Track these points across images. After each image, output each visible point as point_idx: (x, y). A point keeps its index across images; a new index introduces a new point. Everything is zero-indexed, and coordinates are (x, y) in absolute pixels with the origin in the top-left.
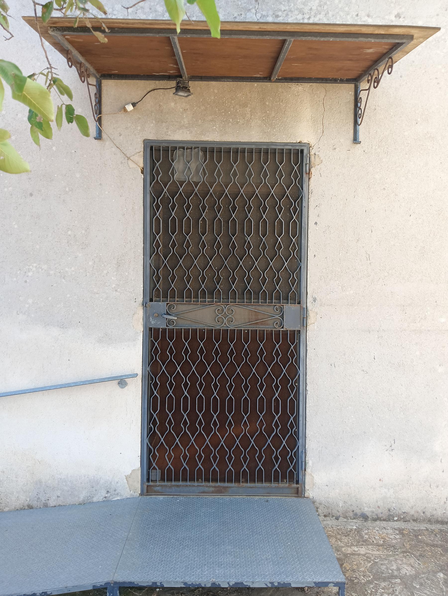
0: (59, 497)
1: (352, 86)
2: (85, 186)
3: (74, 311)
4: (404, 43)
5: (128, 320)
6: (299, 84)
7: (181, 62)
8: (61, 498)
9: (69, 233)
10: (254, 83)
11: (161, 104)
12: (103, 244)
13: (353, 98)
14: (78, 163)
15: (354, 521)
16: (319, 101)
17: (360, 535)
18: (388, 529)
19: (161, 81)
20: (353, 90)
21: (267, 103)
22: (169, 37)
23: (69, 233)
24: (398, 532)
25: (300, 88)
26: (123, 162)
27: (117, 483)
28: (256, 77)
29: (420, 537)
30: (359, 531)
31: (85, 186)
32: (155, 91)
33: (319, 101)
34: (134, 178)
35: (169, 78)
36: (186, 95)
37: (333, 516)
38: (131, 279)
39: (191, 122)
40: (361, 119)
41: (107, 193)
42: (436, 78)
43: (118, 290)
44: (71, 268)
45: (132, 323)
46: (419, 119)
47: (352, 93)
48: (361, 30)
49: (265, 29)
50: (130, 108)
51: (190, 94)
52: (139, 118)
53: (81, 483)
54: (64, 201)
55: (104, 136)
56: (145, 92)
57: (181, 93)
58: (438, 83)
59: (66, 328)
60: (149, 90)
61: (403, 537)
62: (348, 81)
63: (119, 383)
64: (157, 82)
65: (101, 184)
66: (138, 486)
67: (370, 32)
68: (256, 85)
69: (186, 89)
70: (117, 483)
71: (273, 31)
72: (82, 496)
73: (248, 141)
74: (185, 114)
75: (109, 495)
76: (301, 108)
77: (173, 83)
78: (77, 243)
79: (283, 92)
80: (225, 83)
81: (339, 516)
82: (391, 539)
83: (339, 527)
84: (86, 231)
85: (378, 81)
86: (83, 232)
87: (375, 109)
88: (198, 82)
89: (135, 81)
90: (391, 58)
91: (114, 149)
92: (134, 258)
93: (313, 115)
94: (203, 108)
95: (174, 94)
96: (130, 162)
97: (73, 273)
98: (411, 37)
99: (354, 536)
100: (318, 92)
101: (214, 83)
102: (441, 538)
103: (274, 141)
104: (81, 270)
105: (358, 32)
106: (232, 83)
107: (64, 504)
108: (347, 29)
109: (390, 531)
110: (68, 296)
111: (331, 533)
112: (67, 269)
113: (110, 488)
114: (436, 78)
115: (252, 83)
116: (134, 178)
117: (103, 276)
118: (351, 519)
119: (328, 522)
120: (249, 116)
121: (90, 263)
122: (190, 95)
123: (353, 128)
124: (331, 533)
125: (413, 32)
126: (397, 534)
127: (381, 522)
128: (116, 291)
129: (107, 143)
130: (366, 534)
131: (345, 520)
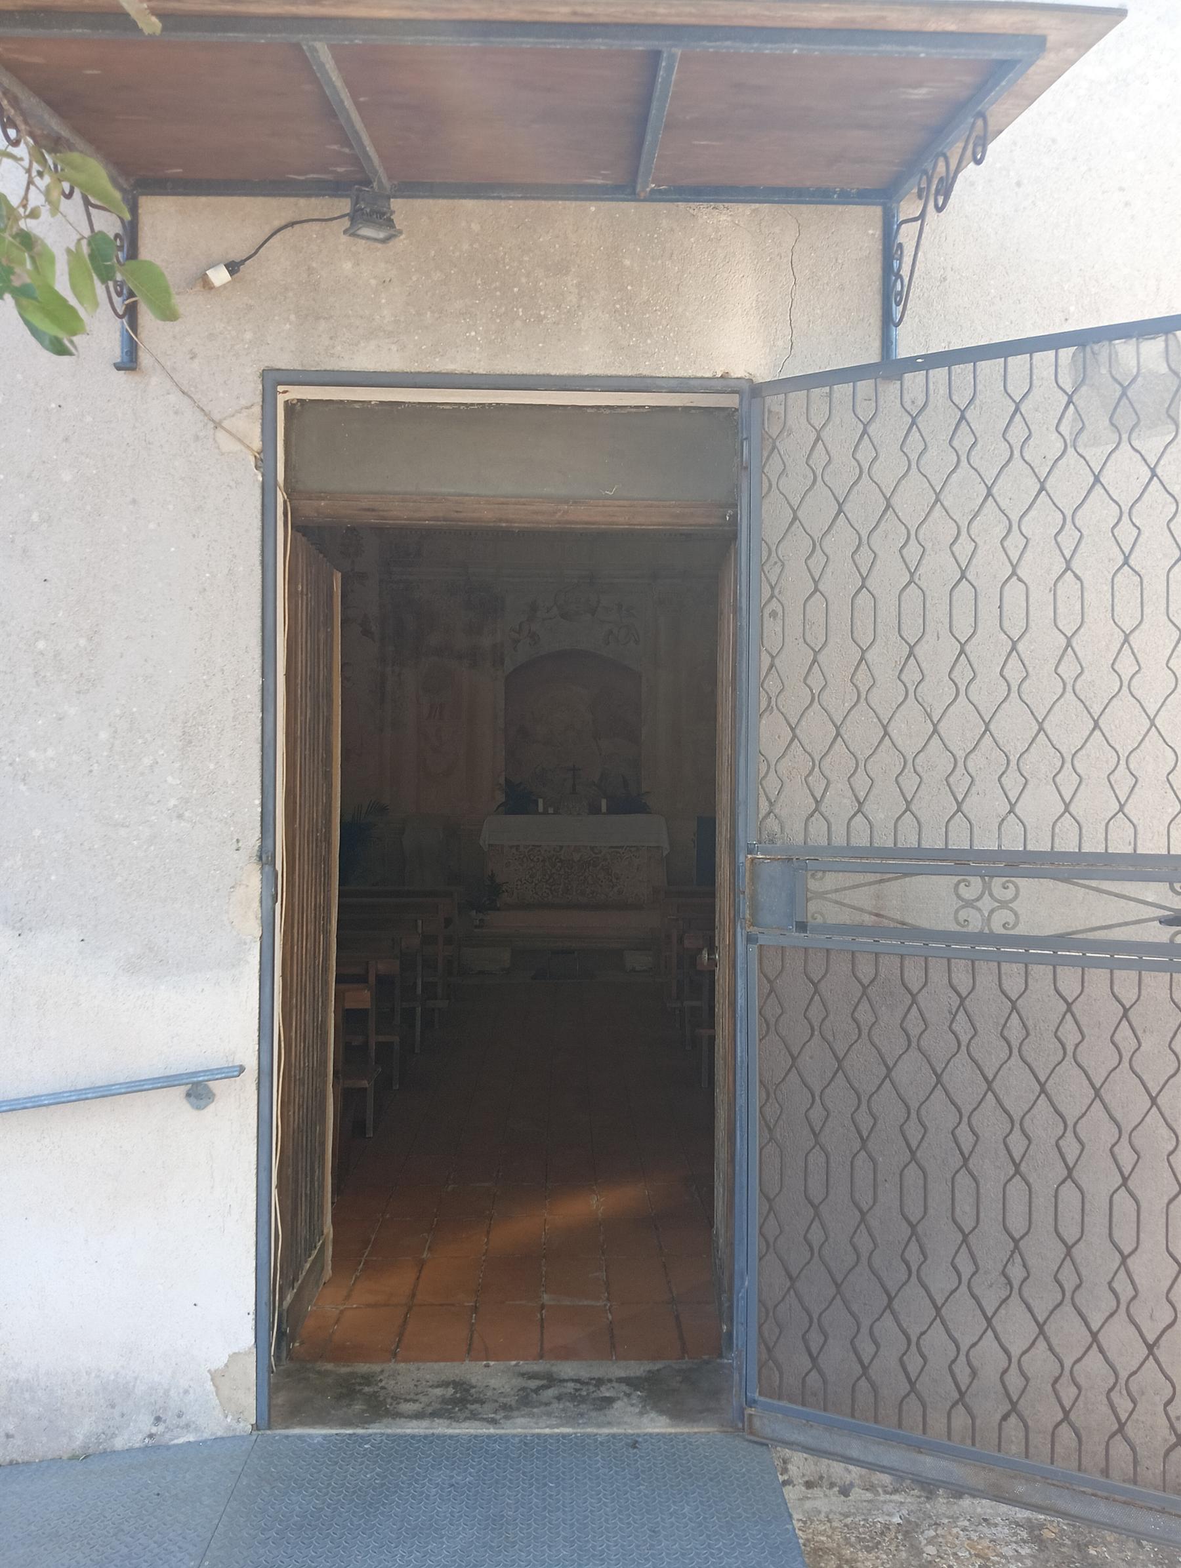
0: (13, 1436)
1: (877, 211)
2: (88, 508)
3: (53, 878)
4: (1019, 61)
5: (215, 903)
6: (721, 205)
7: (356, 132)
8: (18, 1441)
9: (41, 645)
10: (588, 203)
11: (314, 265)
12: (140, 679)
13: (878, 246)
14: (66, 440)
15: (896, 1497)
16: (779, 255)
17: (912, 1545)
18: (996, 1525)
19: (313, 200)
20: (879, 224)
21: (627, 262)
22: (297, 46)
23: (41, 645)
24: (1025, 1535)
25: (723, 218)
26: (201, 434)
27: (186, 1392)
28: (592, 186)
29: (1092, 1552)
30: (908, 1530)
31: (88, 508)
32: (297, 227)
33: (779, 255)
34: (232, 484)
35: (335, 188)
36: (382, 235)
37: (832, 1485)
38: (226, 782)
39: (402, 319)
40: (901, 308)
41: (152, 526)
42: (1121, 189)
43: (187, 814)
44: (45, 750)
45: (227, 912)
46: (1072, 309)
47: (876, 232)
48: (883, 18)
49: (590, 15)
50: (219, 276)
51: (392, 232)
52: (250, 308)
53: (79, 1394)
54: (24, 551)
55: (145, 359)
56: (268, 231)
57: (366, 231)
58: (1127, 204)
59: (30, 930)
60: (277, 224)
61: (1040, 1550)
62: (863, 197)
63: (188, 1095)
64: (302, 202)
65: (134, 502)
66: (249, 1401)
67: (913, 26)
68: (593, 209)
69: (381, 218)
70: (186, 1392)
71: (617, 25)
72: (81, 1434)
73: (571, 372)
74: (383, 295)
75: (161, 1428)
76: (726, 275)
77: (344, 205)
78: (64, 677)
79: (672, 230)
80: (503, 203)
81: (852, 1485)
82: (1005, 1557)
83: (849, 1520)
84: (90, 639)
85: (946, 189)
86: (83, 642)
87: (945, 279)
88: (426, 201)
89: (235, 199)
90: (982, 115)
91: (175, 398)
92: (235, 718)
93: (761, 298)
94: (437, 276)
95: (345, 232)
96: (221, 435)
97: (52, 765)
98: (1039, 43)
99: (893, 1548)
100: (777, 230)
101: (469, 204)
102: (1156, 1554)
103: (646, 372)
104: (75, 758)
105: (877, 26)
106: (522, 204)
107: (26, 1458)
108: (840, 15)
109: (1003, 1532)
110: (37, 833)
111: (824, 1539)
112: (32, 754)
113: (165, 1409)
114: (1121, 189)
115: (583, 203)
116: (232, 484)
117: (142, 774)
118: (886, 1492)
119: (818, 1504)
120: (573, 298)
121: (103, 735)
122: (394, 236)
123: (880, 333)
124: (824, 1539)
125: (1046, 25)
126: (1025, 1542)
127: (976, 1501)
128: (180, 816)
129: (154, 380)
130: (930, 1542)
131: (869, 1495)
